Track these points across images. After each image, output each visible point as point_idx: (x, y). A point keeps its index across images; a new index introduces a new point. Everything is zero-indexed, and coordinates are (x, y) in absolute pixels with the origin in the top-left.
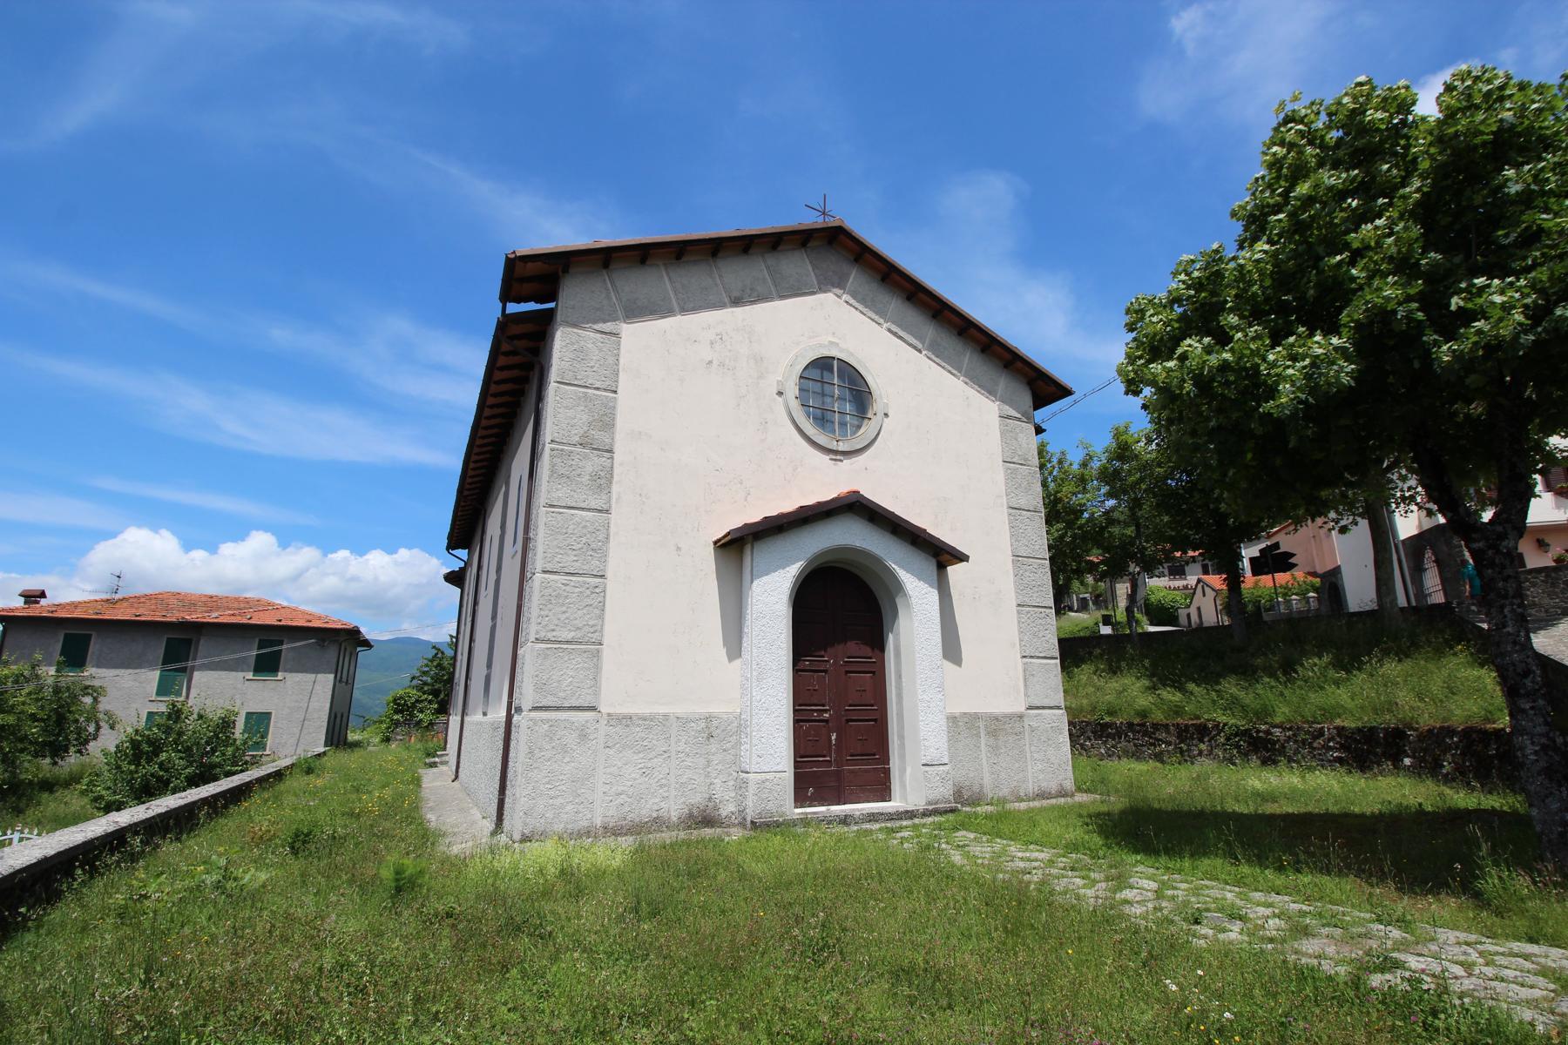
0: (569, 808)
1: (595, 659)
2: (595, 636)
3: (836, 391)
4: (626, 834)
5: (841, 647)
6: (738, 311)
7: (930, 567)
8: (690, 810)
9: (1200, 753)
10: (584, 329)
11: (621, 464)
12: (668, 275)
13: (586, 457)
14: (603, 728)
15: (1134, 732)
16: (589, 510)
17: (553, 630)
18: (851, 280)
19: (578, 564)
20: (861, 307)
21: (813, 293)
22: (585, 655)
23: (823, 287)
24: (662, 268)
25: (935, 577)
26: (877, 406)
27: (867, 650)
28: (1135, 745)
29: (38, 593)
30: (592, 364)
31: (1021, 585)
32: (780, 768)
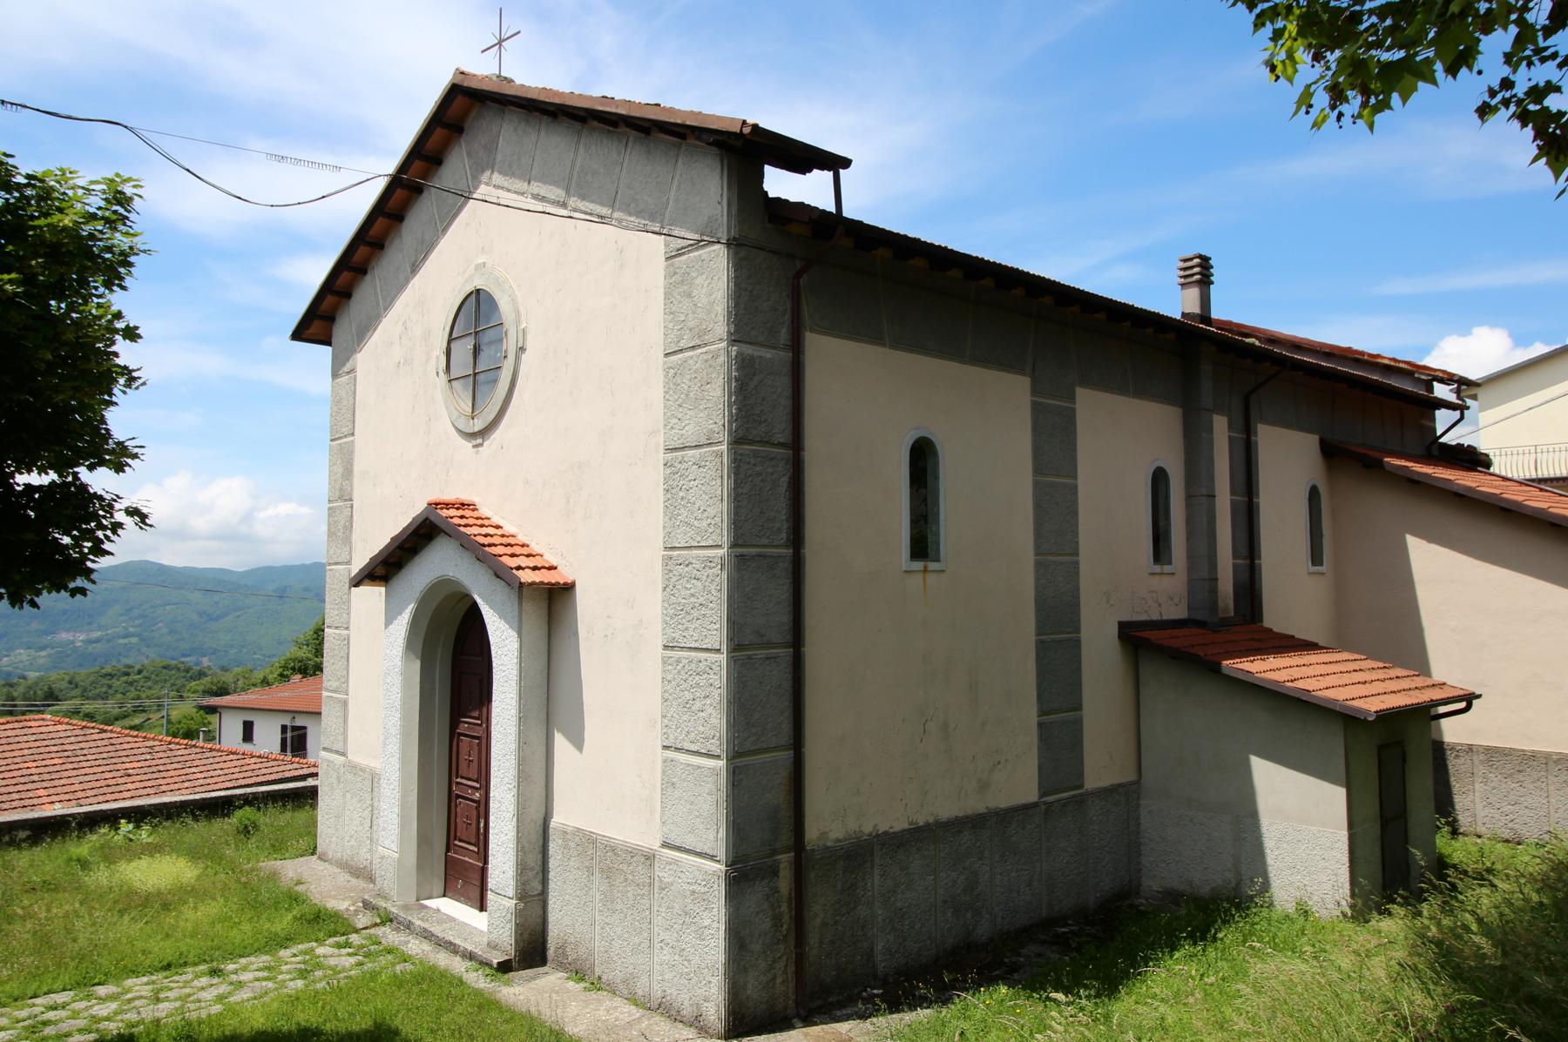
25: (516, 613)
31: (675, 613)
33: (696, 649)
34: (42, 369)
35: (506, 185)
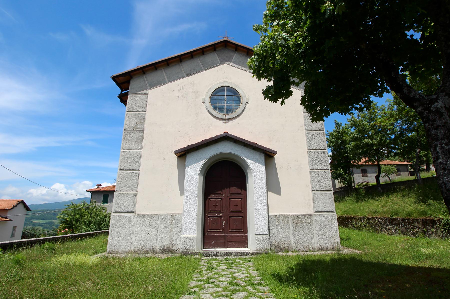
2: (135, 189)
4: (141, 254)
5: (228, 189)
6: (189, 78)
8: (164, 247)
9: (433, 233)
10: (137, 94)
11: (146, 134)
12: (165, 71)
13: (135, 133)
14: (136, 219)
15: (405, 222)
16: (135, 149)
18: (234, 58)
20: (238, 66)
21: (218, 66)
22: (131, 195)
23: (222, 63)
24: (163, 70)
26: (243, 101)
27: (239, 190)
28: (406, 229)
29: (99, 185)
32: (193, 234)
33: (319, 169)
34: (291, 78)
35: (238, 67)
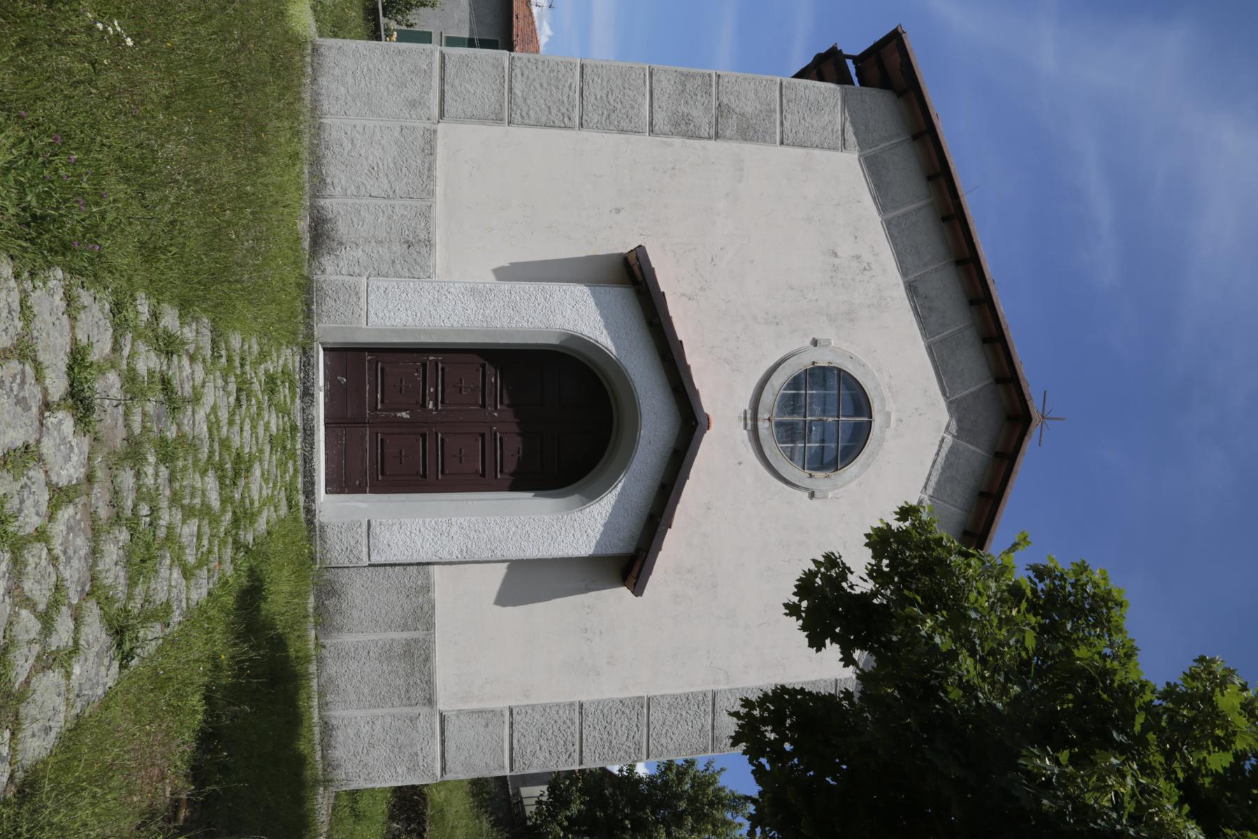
0: (342, 90)
1: (493, 116)
2: (518, 117)
3: (830, 419)
6: (900, 292)
7: (621, 545)
8: (331, 219)
10: (843, 111)
11: (704, 148)
13: (707, 110)
14: (421, 125)
16: (651, 112)
17: (522, 75)
18: (972, 447)
19: (592, 99)
20: (941, 459)
21: (944, 393)
22: (497, 106)
23: (955, 406)
26: (820, 480)
27: (511, 466)
30: (808, 119)
32: (371, 315)
33: (581, 733)
